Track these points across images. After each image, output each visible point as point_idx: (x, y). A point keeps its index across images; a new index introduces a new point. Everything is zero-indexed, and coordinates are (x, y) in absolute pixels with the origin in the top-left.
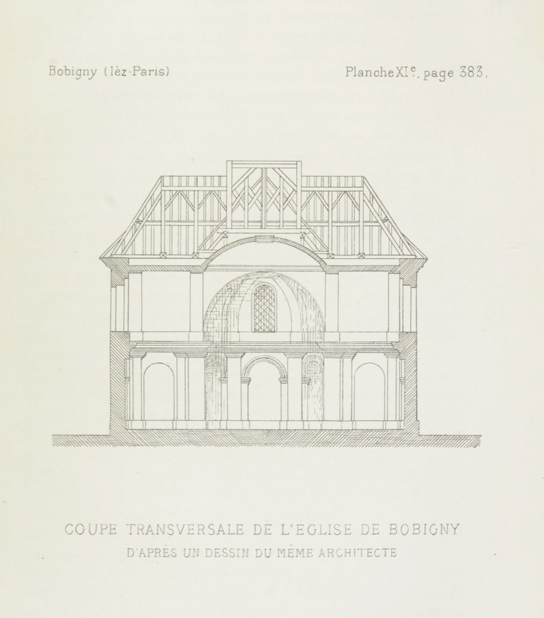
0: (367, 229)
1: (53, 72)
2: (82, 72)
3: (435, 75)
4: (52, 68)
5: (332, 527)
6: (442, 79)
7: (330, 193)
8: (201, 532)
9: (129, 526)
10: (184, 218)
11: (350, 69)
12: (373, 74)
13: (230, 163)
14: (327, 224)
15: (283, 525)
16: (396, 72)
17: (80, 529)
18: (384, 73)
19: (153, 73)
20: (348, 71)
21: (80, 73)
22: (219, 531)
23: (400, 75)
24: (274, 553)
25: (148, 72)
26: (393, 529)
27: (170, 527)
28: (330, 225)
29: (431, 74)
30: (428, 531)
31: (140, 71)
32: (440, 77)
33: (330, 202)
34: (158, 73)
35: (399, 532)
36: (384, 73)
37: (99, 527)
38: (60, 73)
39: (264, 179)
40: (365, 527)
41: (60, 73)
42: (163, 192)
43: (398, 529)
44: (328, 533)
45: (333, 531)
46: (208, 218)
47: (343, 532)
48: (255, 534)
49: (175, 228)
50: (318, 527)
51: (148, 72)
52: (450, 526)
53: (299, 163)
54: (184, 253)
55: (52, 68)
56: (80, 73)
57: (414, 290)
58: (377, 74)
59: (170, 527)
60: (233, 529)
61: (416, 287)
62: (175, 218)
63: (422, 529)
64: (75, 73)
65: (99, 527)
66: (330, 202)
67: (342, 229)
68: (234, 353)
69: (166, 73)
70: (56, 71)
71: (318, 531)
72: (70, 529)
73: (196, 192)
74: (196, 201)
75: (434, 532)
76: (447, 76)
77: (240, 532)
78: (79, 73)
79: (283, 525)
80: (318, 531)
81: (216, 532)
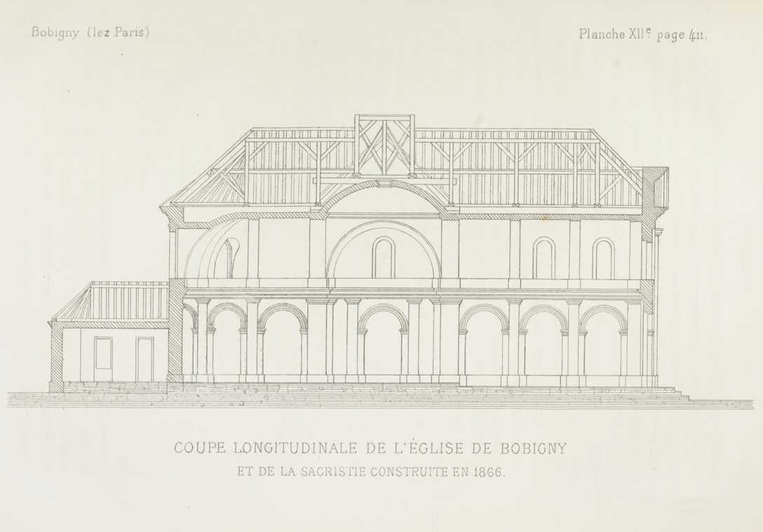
0: (521, 177)
2: (65, 33)
4: (36, 29)
5: (444, 445)
6: (61, 38)
7: (517, 144)
10: (488, 167)
13: (357, 117)
14: (513, 172)
15: (396, 444)
19: (133, 34)
21: (62, 35)
23: (633, 37)
24: (255, 472)
26: (505, 448)
28: (575, 173)
30: (537, 451)
31: (122, 33)
32: (59, 37)
33: (451, 154)
34: (138, 34)
36: (615, 35)
37: (207, 445)
39: (385, 130)
41: (43, 34)
42: (247, 144)
43: (510, 448)
44: (439, 451)
45: (445, 448)
46: (289, 166)
47: (455, 451)
49: (504, 177)
50: (429, 446)
51: (129, 34)
52: (557, 445)
53: (412, 117)
54: (473, 202)
56: (62, 35)
58: (609, 36)
60: (346, 447)
62: (466, 166)
64: (58, 34)
65: (207, 445)
66: (451, 154)
67: (504, 177)
68: (311, 290)
71: (274, 450)
72: (179, 448)
73: (575, 145)
74: (517, 153)
75: (424, 451)
76: (678, 37)
77: (353, 450)
78: (674, 36)
79: (396, 444)
80: (429, 450)
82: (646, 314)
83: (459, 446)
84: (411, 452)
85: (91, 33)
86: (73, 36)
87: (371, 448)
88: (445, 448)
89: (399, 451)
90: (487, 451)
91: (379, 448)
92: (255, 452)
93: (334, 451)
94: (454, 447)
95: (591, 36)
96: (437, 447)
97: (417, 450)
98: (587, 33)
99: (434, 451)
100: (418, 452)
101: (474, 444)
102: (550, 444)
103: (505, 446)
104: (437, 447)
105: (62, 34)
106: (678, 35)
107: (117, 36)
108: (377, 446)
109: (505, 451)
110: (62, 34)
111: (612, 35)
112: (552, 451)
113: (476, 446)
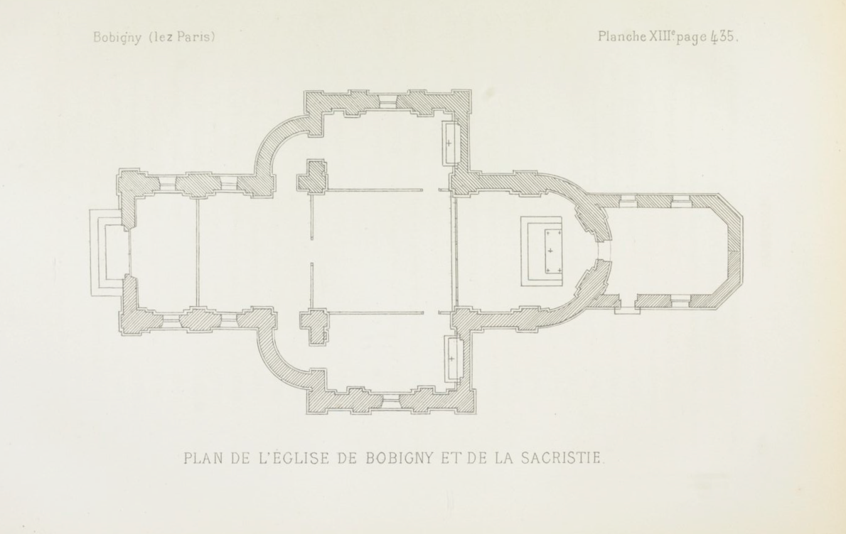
1: (97, 39)
3: (688, 38)
8: (556, 460)
9: (579, 454)
11: (602, 34)
12: (625, 38)
16: (649, 36)
17: (381, 458)
18: (636, 38)
20: (179, 37)
22: (533, 459)
23: (654, 39)
25: (192, 38)
27: (571, 454)
29: (684, 37)
31: (185, 37)
32: (692, 41)
35: (375, 460)
38: (105, 39)
40: (235, 455)
41: (105, 39)
43: (375, 457)
44: (304, 461)
45: (309, 458)
47: (320, 461)
48: (368, 463)
50: (293, 456)
51: (192, 38)
52: (424, 454)
55: (602, 34)
57: (623, 198)
59: (571, 454)
61: (620, 195)
63: (398, 458)
69: (211, 39)
70: (101, 36)
79: (497, 453)
80: (294, 461)
81: (531, 460)
82: (165, 325)
83: (483, 455)
84: (443, 463)
85: (153, 38)
86: (136, 42)
87: (236, 459)
88: (309, 458)
89: (263, 461)
90: (325, 460)
91: (351, 458)
92: (417, 463)
93: (535, 461)
94: (319, 457)
95: (610, 39)
96: (301, 457)
97: (281, 459)
98: (606, 36)
99: (299, 461)
100: (282, 461)
101: (340, 454)
102: (216, 453)
103: (370, 455)
104: (301, 457)
105: (695, 38)
106: (699, 37)
107: (600, 40)
108: (478, 456)
109: (370, 460)
110: (695, 38)
111: (632, 37)
112: (419, 461)
113: (342, 455)
